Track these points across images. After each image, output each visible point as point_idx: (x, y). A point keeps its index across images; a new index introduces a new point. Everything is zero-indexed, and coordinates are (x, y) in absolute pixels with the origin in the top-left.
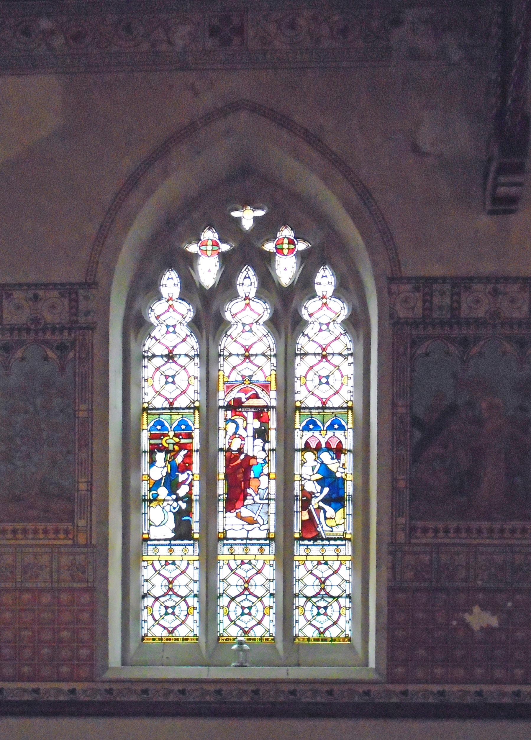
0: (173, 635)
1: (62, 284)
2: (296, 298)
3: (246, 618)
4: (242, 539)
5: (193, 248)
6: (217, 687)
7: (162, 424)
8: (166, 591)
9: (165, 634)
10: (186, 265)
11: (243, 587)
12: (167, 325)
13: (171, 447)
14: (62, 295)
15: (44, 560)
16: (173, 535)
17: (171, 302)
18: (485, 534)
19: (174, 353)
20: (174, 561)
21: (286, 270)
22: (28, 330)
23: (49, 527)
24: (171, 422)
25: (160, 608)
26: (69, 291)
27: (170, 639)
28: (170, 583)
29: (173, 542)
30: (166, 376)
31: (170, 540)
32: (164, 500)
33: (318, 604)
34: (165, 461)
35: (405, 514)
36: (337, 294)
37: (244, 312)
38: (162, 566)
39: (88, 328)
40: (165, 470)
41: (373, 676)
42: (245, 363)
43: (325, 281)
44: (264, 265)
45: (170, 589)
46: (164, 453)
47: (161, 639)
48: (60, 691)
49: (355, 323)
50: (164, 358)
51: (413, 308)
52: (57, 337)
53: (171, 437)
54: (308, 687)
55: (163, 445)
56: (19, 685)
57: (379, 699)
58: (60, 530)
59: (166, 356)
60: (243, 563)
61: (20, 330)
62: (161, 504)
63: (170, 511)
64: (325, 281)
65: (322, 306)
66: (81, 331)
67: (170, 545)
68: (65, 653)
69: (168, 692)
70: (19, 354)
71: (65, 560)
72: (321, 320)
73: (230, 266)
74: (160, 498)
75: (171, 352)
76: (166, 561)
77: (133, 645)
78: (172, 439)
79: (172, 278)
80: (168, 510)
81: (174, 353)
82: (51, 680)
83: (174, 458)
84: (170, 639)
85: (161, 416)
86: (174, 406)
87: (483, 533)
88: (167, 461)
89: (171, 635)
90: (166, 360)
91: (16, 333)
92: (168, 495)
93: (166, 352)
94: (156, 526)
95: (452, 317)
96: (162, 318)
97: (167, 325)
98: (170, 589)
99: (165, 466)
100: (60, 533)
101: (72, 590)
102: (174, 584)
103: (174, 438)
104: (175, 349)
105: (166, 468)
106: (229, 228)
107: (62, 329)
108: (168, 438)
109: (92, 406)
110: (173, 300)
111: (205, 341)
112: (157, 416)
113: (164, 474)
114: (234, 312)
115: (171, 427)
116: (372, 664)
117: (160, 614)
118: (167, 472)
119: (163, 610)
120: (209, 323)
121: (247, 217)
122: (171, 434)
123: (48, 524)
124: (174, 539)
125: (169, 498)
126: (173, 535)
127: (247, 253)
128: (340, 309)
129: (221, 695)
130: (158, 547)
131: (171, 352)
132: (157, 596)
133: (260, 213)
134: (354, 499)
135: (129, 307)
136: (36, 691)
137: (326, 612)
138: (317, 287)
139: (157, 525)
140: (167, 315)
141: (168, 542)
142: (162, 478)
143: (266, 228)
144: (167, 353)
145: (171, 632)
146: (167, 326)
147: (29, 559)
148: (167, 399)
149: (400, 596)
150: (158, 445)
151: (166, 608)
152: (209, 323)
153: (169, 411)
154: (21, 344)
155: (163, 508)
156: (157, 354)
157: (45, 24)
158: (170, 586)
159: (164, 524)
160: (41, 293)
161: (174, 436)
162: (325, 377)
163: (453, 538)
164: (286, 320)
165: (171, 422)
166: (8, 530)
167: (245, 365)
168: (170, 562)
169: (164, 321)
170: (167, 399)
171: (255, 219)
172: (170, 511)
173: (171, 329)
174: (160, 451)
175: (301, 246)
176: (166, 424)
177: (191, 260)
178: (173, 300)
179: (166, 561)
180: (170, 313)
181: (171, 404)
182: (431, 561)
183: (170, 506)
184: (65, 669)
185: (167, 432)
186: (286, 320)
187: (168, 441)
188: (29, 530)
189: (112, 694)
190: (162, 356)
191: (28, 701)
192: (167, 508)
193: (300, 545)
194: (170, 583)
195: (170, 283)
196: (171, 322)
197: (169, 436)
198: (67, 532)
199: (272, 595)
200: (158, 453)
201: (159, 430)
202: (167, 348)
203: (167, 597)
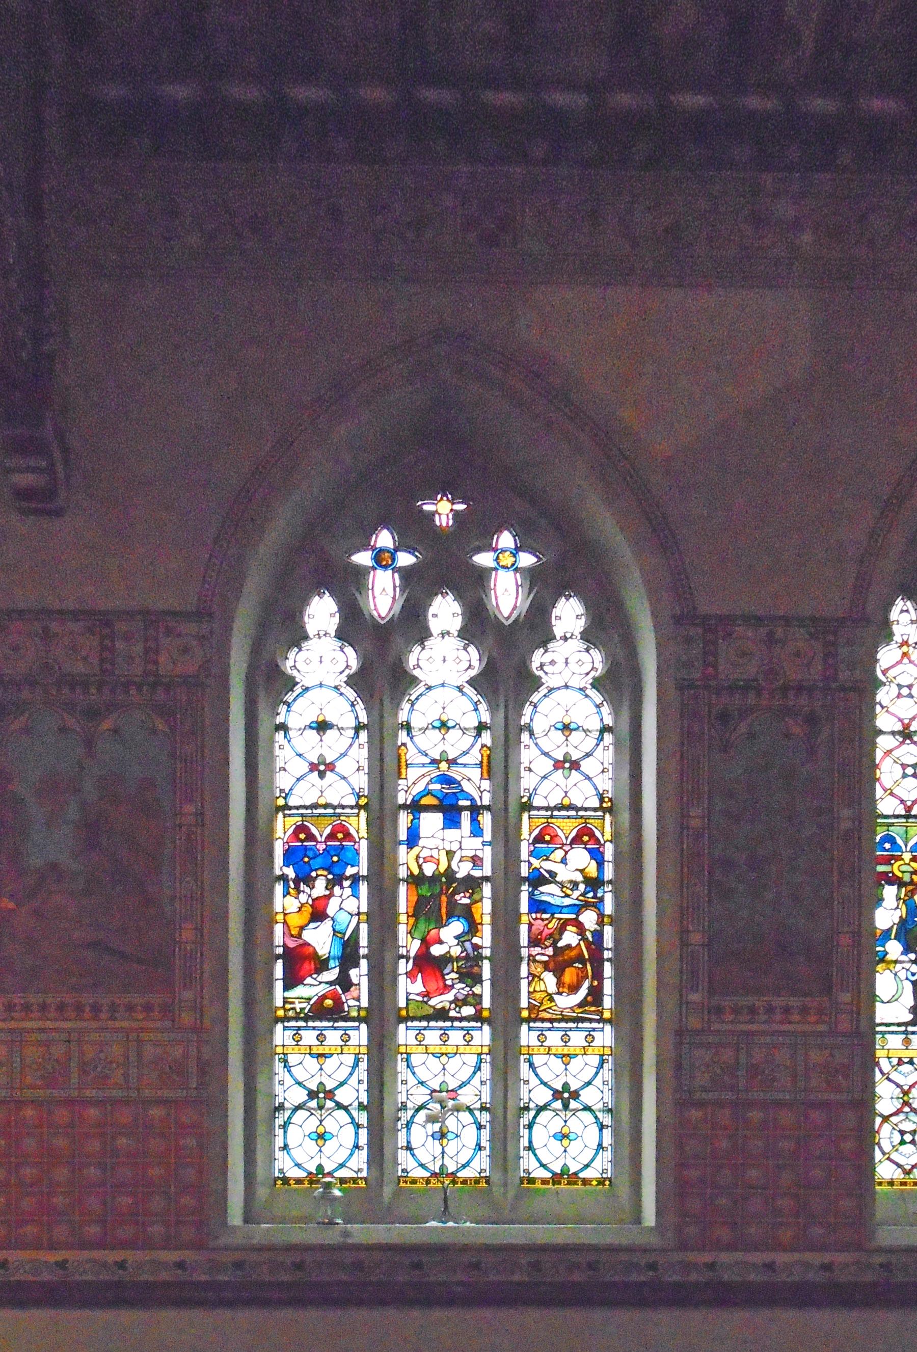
0: (911, 1176)
1: (813, 619)
2: (398, 640)
3: (444, 1149)
4: (899, 1025)
5: (484, 559)
6: (238, 1256)
7: (892, 840)
8: (899, 1106)
9: (898, 1175)
10: (348, 587)
11: (901, 1101)
12: (899, 685)
13: (907, 878)
14: (90, 630)
15: (783, 1056)
16: (911, 1017)
17: (905, 649)
18: (156, 1014)
19: (912, 729)
20: (911, 1058)
21: (507, 596)
22: (759, 691)
23: (49, 1000)
24: (906, 838)
25: (891, 1133)
26: (826, 629)
27: (905, 1184)
28: (906, 1093)
29: (910, 1029)
30: (902, 765)
31: (906, 1024)
32: (896, 962)
33: (903, 1127)
34: (898, 899)
35: (700, 987)
36: (588, 637)
37: (900, 666)
38: (893, 1067)
39: (854, 689)
40: (898, 913)
41: (654, 1240)
42: (904, 746)
43: (569, 615)
44: (472, 587)
45: (906, 1103)
46: (896, 886)
47: (891, 1183)
48: (158, 1265)
49: (618, 684)
50: (897, 737)
51: (809, 665)
52: (803, 700)
53: (907, 861)
54: (377, 1255)
55: (893, 874)
56: (739, 1256)
57: (788, 1277)
58: (15, 1005)
59: (899, 733)
60: (900, 1062)
61: (746, 689)
62: (891, 968)
63: (907, 979)
64: (569, 615)
65: (902, 658)
66: (692, 692)
67: (906, 1032)
68: (157, 1203)
69: (632, 1266)
70: (743, 728)
71: (816, 1056)
72: (900, 680)
73: (417, 589)
74: (889, 957)
75: (906, 727)
76: (900, 1059)
77: (262, 1192)
78: (909, 864)
79: (907, 611)
80: (903, 977)
81: (912, 729)
82: (731, 1247)
83: (912, 897)
84: (905, 1184)
85: (891, 828)
86: (913, 813)
87: (84, 1011)
88: (900, 899)
89: (907, 1177)
90: (901, 739)
91: (791, 694)
92: (902, 954)
93: (898, 727)
94: (883, 1002)
95: (146, 673)
96: (891, 674)
97: (899, 685)
98: (906, 1103)
99: (897, 908)
100: (50, 1012)
101: (825, 1105)
102: (911, 1096)
103: (912, 864)
104: (913, 723)
105: (898, 910)
106: (415, 529)
107: (746, 689)
108: (902, 862)
109: (202, 807)
110: (908, 646)
111: (377, 707)
112: (886, 828)
113: (897, 921)
114: (884, 667)
115: (906, 846)
116: (649, 1217)
117: (891, 1142)
118: (901, 917)
119: (897, 1138)
120: (382, 677)
121: (443, 510)
122: (907, 857)
123: (792, 999)
124: (912, 1023)
125: (904, 958)
126: (911, 1017)
127: (445, 567)
128: (595, 661)
129: (65, 1269)
130: (887, 1036)
131: (906, 727)
132: (886, 1114)
133: (461, 507)
134: (521, 959)
135: (257, 649)
136: (770, 1266)
137: (913, 1139)
138: (895, 628)
139: (885, 1001)
140: (899, 668)
141: (903, 1028)
142: (892, 927)
143: (476, 529)
144: (901, 728)
145: (908, 1172)
146: (900, 686)
147: (90, 1053)
148: (902, 801)
149: (695, 1114)
150: (886, 873)
151: (902, 1133)
152: (382, 677)
153: (904, 820)
154: (745, 712)
155: (895, 975)
156: (884, 730)
157: (784, 209)
158: (906, 1098)
159: (896, 1000)
160: (54, 627)
161: (911, 860)
162: (904, 770)
163: (764, 1023)
164: (506, 678)
165: (906, 838)
166: (776, 1007)
167: (905, 748)
168: (906, 1060)
169: (895, 678)
170: (902, 801)
171: (457, 514)
172: (907, 979)
173: (905, 691)
174: (891, 883)
175: (405, 559)
176: (899, 841)
177: (482, 576)
178: (908, 646)
179: (900, 1059)
180: (321, 660)
181: (909, 809)
182: (186, 1055)
183: (908, 970)
184: (156, 1230)
185: (900, 854)
186: (506, 678)
187: (904, 868)
188: (776, 1007)
189: (832, 1271)
190: (893, 733)
191: (147, 1282)
192: (902, 975)
193: (285, 1028)
194: (906, 1093)
195: (322, 613)
196: (904, 680)
197: (902, 859)
198: (820, 1011)
199: (610, 1110)
200: (886, 886)
201: (887, 851)
202: (901, 720)
203: (902, 1116)
